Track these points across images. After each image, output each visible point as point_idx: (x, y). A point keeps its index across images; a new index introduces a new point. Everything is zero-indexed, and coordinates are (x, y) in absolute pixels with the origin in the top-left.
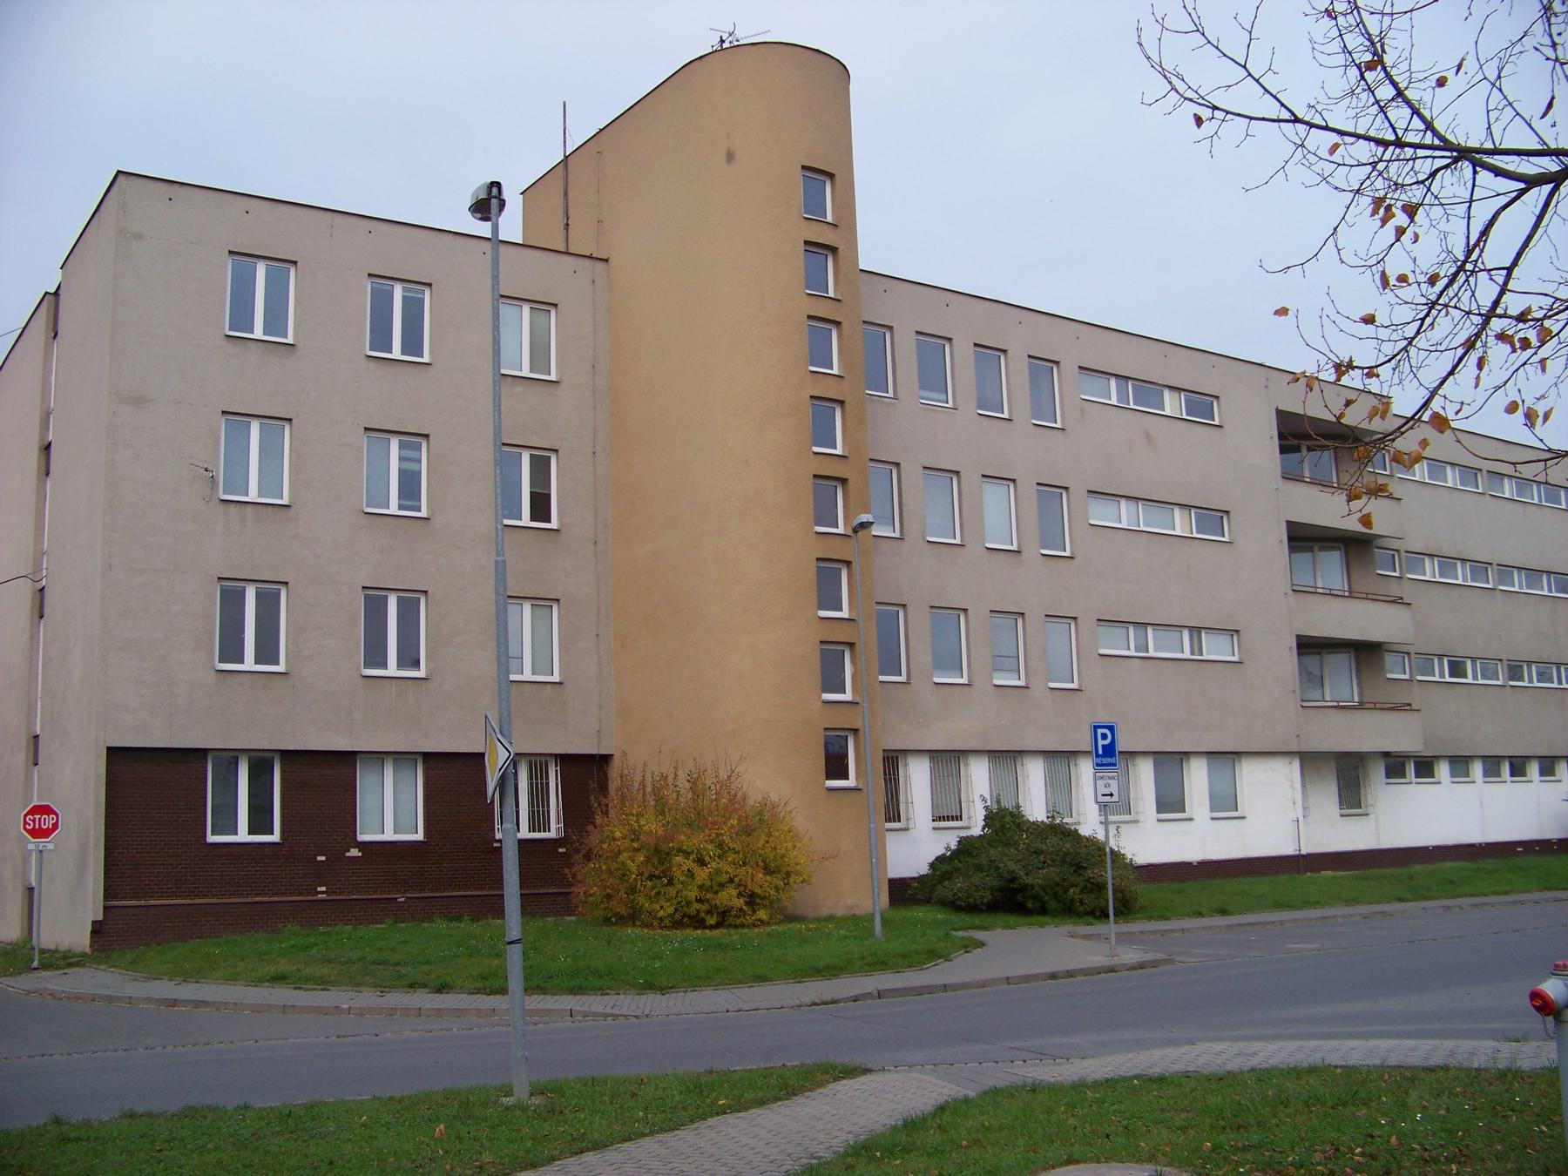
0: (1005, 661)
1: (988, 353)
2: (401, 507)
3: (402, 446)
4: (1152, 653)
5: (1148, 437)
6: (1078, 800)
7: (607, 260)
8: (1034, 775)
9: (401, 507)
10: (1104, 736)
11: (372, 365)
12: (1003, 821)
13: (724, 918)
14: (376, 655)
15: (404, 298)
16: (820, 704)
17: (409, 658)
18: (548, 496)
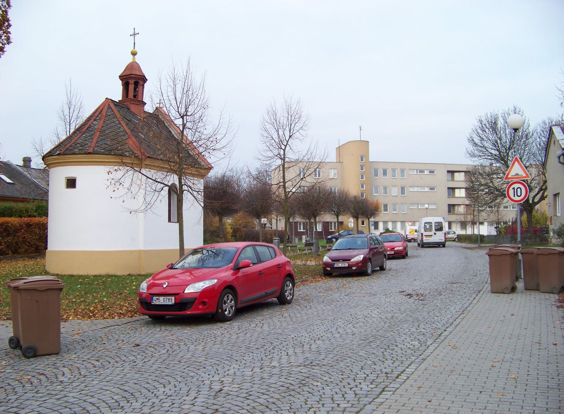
4: (420, 208)
8: (399, 225)
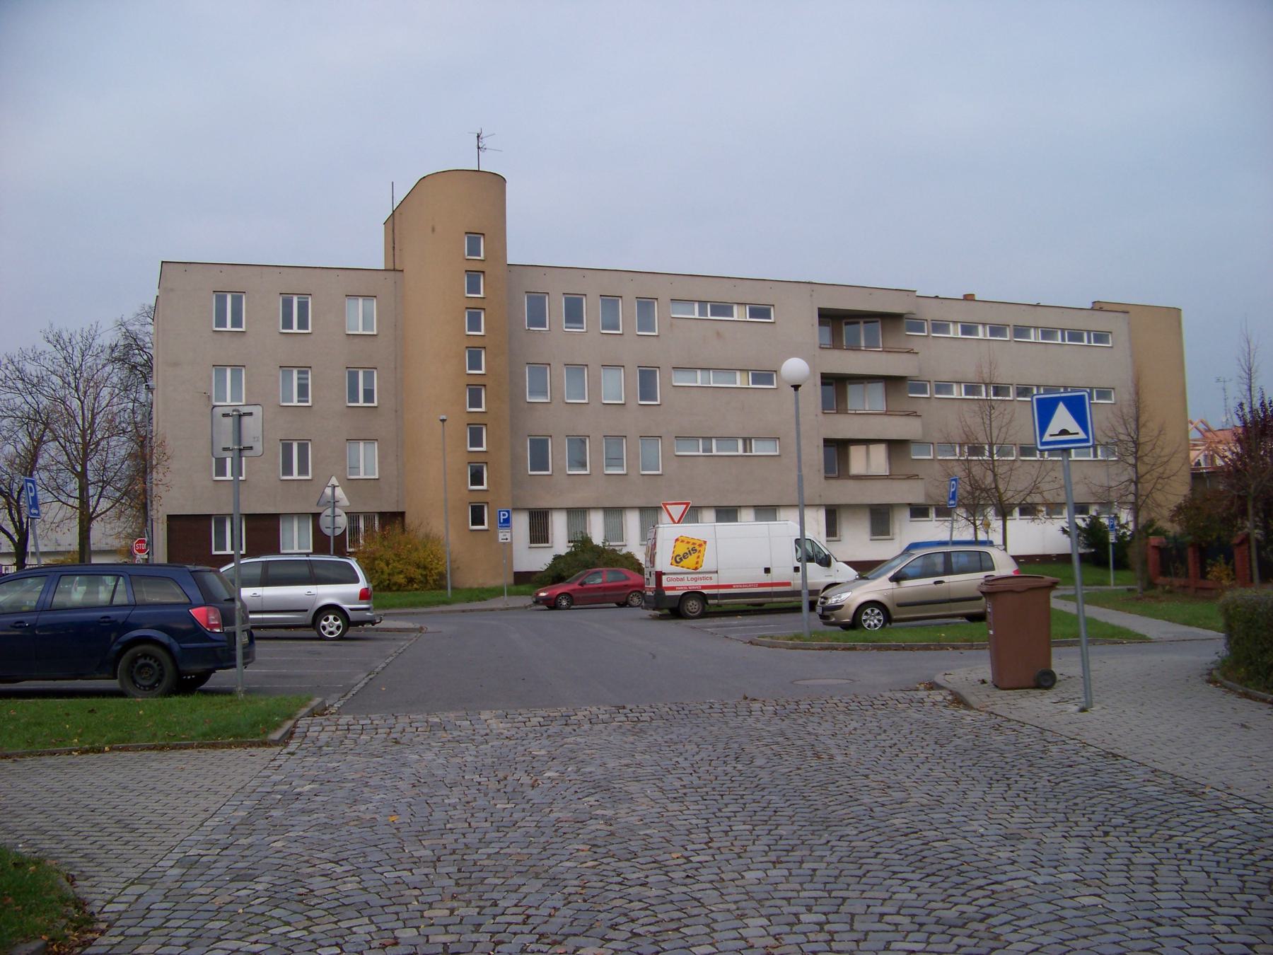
0: (615, 460)
1: (610, 301)
2: (299, 401)
3: (299, 372)
5: (718, 334)
6: (552, 534)
7: (402, 271)
8: (632, 522)
9: (299, 401)
10: (504, 515)
11: (283, 336)
12: (582, 543)
13: (400, 588)
14: (287, 469)
15: (298, 302)
16: (467, 492)
17: (303, 469)
18: (373, 391)
